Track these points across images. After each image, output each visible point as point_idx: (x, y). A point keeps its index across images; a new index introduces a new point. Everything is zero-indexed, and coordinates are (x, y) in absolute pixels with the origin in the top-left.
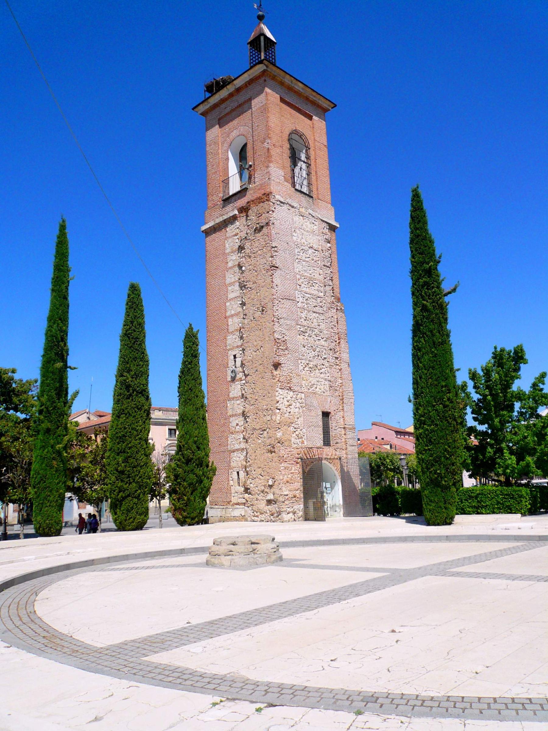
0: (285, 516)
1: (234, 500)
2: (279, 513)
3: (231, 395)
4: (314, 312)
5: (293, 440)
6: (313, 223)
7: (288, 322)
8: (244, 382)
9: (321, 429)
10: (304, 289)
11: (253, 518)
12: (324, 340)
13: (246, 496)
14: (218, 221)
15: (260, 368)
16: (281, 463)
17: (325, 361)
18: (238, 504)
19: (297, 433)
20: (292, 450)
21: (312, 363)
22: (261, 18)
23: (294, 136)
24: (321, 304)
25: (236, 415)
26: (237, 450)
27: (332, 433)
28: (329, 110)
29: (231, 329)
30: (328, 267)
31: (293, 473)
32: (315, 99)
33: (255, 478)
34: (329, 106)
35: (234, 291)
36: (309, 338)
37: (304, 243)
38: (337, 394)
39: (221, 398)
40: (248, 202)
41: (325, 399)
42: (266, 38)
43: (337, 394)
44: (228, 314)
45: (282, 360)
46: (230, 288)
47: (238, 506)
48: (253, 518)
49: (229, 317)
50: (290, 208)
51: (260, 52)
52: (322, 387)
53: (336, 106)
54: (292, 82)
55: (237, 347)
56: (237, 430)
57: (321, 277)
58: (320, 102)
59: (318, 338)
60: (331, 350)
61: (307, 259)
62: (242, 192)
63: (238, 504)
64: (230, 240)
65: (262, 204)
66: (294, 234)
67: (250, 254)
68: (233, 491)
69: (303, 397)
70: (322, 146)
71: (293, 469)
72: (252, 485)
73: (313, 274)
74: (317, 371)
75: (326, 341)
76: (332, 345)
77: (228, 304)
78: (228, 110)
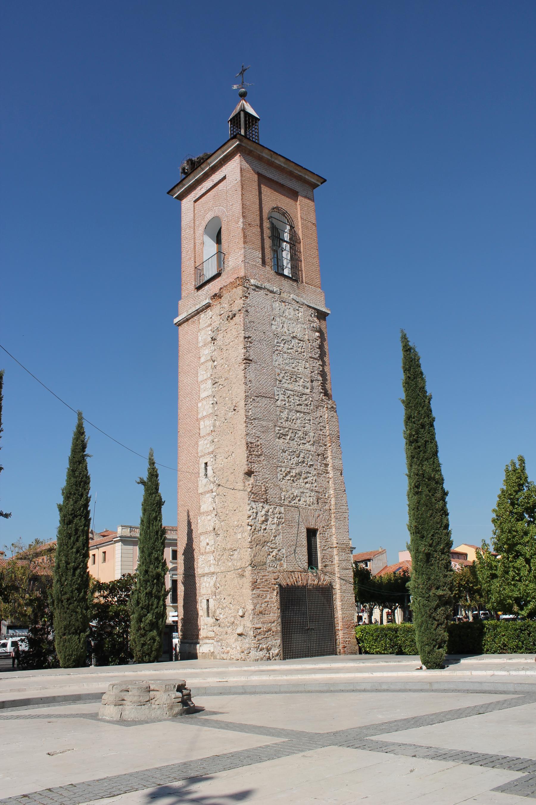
3: (202, 511)
4: (298, 412)
6: (298, 310)
7: (264, 423)
10: (286, 385)
11: (222, 655)
12: (310, 443)
14: (190, 311)
17: (312, 469)
19: (274, 554)
20: (267, 574)
21: (294, 471)
22: (243, 95)
23: (276, 215)
24: (306, 402)
25: (206, 533)
26: (207, 574)
28: (318, 185)
31: (268, 602)
32: (300, 174)
33: (225, 608)
34: (318, 181)
35: (206, 390)
36: (291, 442)
37: (285, 332)
40: (221, 288)
42: (247, 114)
44: (200, 416)
46: (202, 387)
47: (207, 641)
48: (222, 655)
50: (268, 293)
51: (240, 128)
53: (325, 181)
54: (271, 157)
55: (209, 453)
56: (207, 550)
57: (308, 371)
58: (306, 177)
59: (302, 441)
60: (318, 455)
61: (289, 351)
66: (273, 322)
67: (222, 347)
69: (283, 511)
70: (310, 224)
72: (221, 616)
73: (296, 368)
74: (301, 480)
75: (313, 445)
77: (200, 405)
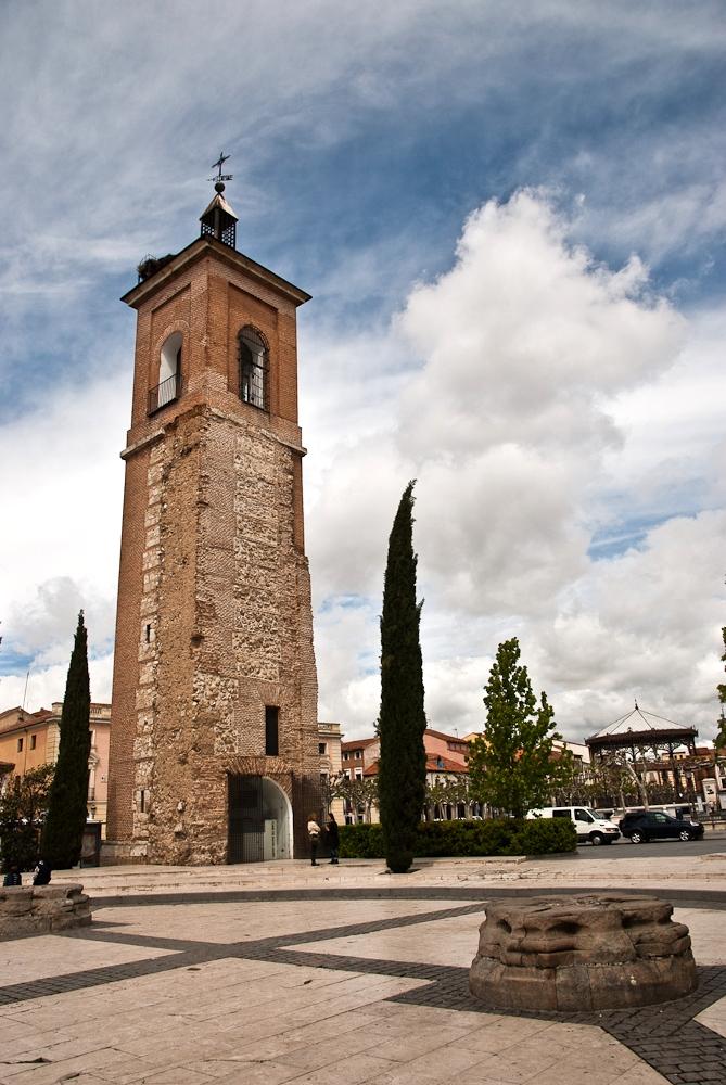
0: (197, 857)
1: (136, 833)
2: (189, 852)
4: (261, 567)
5: (216, 745)
7: (219, 580)
8: (157, 662)
9: (262, 732)
10: (248, 535)
13: (151, 826)
15: (177, 643)
16: (195, 779)
18: (140, 838)
19: (224, 735)
26: (144, 760)
27: (282, 738)
29: (146, 589)
30: (287, 506)
38: (291, 681)
39: (129, 686)
41: (272, 688)
43: (291, 681)
45: (206, 631)
46: (149, 534)
47: (140, 842)
49: (145, 572)
52: (268, 672)
55: (153, 614)
57: (275, 520)
60: (285, 619)
61: (255, 495)
62: (173, 402)
63: (140, 838)
64: (153, 469)
65: (192, 420)
68: (135, 820)
71: (215, 787)
75: (277, 607)
76: (287, 614)
77: (145, 555)
78: (164, 299)
